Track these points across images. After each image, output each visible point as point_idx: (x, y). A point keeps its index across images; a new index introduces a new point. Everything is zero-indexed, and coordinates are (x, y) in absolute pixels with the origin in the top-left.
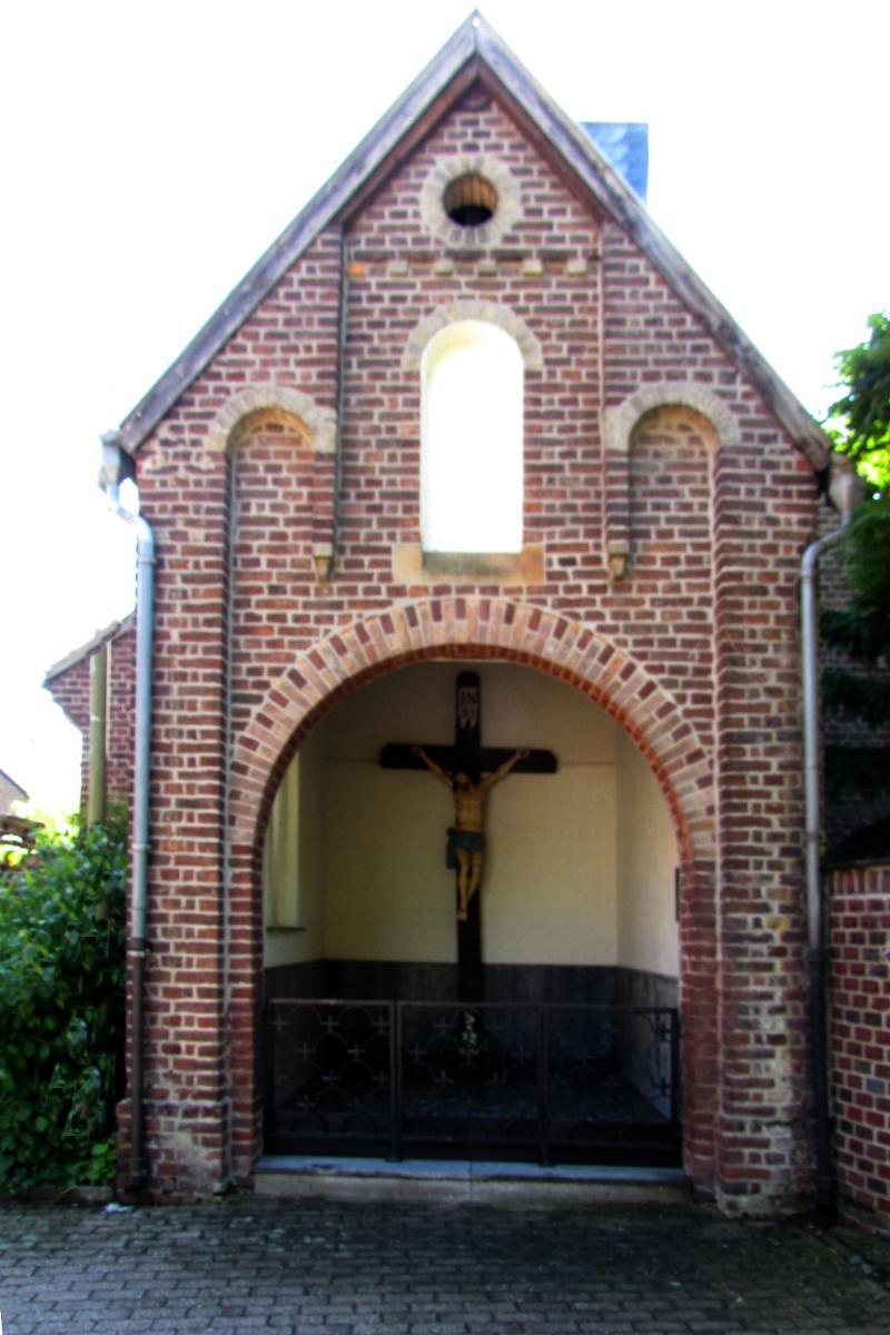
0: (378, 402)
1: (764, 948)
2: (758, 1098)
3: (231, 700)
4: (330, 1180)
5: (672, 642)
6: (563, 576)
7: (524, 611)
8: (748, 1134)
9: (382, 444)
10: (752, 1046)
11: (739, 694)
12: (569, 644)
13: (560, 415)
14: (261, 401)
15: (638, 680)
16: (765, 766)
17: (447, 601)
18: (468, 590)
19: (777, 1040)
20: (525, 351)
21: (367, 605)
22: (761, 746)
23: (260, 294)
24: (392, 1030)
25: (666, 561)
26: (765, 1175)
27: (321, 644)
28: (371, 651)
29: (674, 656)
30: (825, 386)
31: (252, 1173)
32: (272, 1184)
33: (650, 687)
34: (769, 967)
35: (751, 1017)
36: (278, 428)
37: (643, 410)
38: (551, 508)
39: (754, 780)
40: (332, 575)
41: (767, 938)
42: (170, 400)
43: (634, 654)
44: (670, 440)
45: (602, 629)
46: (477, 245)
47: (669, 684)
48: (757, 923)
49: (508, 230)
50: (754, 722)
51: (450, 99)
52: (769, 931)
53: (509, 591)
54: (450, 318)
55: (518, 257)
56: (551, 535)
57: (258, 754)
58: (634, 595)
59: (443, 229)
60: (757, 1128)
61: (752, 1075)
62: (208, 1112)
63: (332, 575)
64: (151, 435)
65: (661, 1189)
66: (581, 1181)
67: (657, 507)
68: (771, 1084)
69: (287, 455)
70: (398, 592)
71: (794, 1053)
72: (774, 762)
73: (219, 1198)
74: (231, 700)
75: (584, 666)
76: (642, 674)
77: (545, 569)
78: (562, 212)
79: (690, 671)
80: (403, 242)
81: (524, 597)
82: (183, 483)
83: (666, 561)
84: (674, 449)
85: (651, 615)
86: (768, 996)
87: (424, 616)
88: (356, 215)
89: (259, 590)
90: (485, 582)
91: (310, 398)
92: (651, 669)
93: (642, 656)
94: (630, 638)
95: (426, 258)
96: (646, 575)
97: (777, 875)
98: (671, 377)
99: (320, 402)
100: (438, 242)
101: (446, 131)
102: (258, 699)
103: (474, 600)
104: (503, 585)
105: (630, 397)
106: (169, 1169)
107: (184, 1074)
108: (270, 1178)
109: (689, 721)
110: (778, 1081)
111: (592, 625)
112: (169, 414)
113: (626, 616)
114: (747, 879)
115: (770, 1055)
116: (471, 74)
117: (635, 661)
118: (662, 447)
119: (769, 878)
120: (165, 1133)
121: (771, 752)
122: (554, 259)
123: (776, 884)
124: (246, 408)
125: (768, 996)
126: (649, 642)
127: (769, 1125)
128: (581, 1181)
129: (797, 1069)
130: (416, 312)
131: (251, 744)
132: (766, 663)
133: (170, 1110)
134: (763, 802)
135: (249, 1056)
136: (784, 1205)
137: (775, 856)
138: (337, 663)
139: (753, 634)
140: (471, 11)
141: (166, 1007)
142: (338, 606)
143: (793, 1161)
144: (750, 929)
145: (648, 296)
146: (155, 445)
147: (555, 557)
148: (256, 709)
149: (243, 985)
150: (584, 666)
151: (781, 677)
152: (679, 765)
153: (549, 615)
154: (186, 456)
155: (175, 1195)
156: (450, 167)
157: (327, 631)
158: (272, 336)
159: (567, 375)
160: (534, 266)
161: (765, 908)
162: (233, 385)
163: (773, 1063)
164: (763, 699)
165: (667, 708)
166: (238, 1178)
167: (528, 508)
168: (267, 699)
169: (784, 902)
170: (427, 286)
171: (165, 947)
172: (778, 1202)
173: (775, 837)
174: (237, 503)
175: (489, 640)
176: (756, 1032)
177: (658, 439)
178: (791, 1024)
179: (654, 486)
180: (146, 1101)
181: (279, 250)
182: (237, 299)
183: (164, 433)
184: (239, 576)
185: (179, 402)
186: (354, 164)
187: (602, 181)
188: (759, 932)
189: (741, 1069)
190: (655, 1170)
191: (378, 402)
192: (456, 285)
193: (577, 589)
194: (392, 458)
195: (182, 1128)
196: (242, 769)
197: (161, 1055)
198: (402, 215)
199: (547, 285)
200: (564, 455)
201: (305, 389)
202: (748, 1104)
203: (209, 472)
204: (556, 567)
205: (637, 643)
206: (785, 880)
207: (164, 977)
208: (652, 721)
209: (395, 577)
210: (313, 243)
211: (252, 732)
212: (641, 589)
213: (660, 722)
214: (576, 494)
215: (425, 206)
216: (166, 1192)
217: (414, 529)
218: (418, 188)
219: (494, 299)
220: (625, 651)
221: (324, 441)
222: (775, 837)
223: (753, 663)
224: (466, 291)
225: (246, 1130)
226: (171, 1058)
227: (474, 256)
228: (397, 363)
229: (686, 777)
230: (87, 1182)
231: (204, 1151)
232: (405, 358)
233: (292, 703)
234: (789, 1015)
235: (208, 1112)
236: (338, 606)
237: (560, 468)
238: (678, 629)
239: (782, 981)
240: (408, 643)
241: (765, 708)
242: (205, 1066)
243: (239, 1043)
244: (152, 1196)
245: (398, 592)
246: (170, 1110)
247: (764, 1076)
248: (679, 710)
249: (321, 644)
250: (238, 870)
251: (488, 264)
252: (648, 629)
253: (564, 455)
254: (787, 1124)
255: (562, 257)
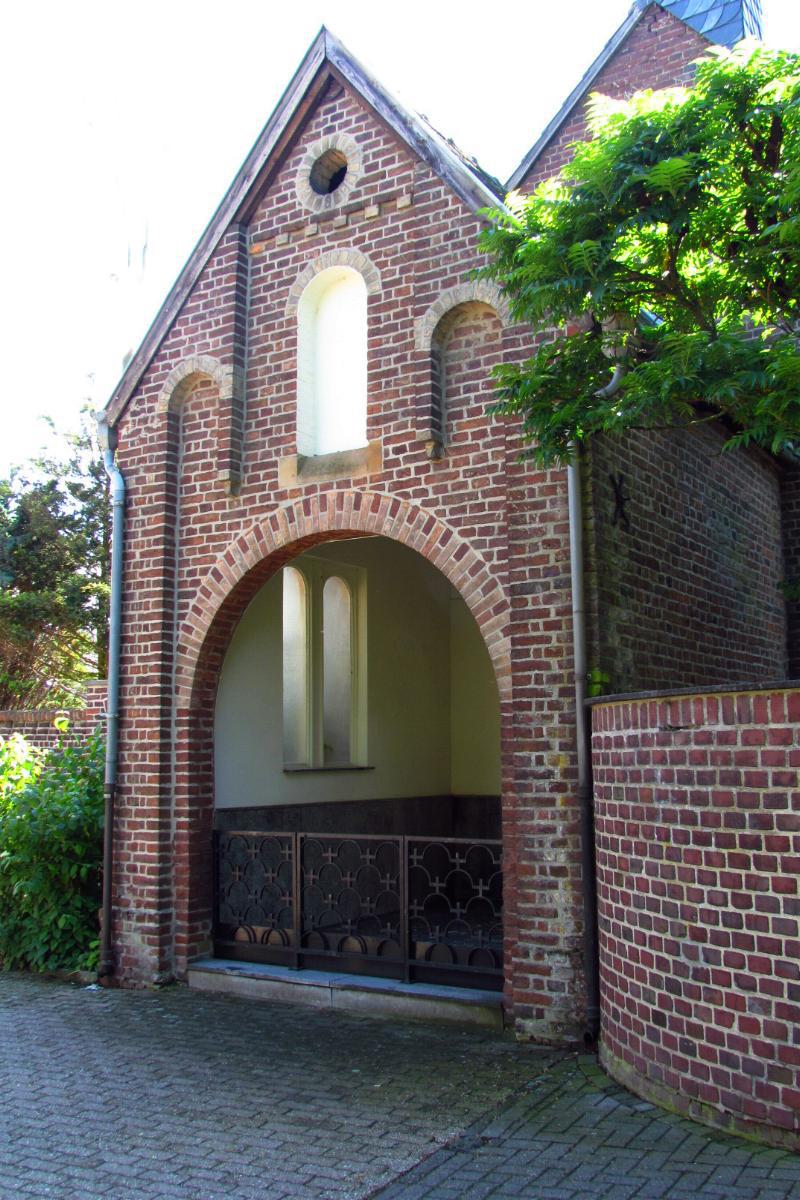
0: (269, 349)
1: (545, 783)
2: (542, 926)
3: (171, 594)
4: (236, 980)
5: (481, 507)
6: (396, 463)
7: (367, 499)
8: (531, 960)
9: (273, 380)
10: (537, 878)
11: (521, 549)
12: (401, 520)
13: (394, 328)
14: (189, 370)
15: (454, 545)
16: (545, 613)
17: (314, 497)
18: (328, 487)
19: (558, 871)
20: (368, 281)
21: (262, 510)
22: (540, 595)
23: (187, 291)
24: (294, 857)
25: (476, 436)
26: (547, 1001)
27: (232, 546)
28: (263, 546)
29: (482, 519)
30: (48, 419)
31: (187, 970)
32: (200, 980)
33: (464, 549)
34: (551, 802)
35: (536, 849)
36: (206, 383)
37: (443, 313)
38: (387, 407)
39: (536, 627)
40: (234, 492)
41: (549, 774)
42: (134, 384)
43: (450, 522)
44: (478, 329)
45: (426, 504)
46: (334, 207)
47: (478, 545)
48: (540, 761)
49: (354, 189)
50: (534, 573)
51: (310, 100)
52: (551, 767)
53: (357, 483)
54: (318, 269)
55: (361, 207)
56: (387, 430)
57: (193, 637)
58: (451, 470)
59: (309, 203)
60: (539, 956)
61: (537, 905)
62: (151, 918)
63: (234, 492)
64: (125, 409)
65: (477, 1009)
66: (411, 996)
67: (468, 390)
68: (555, 915)
69: (211, 403)
70: (282, 496)
71: (574, 884)
72: (552, 608)
73: (157, 987)
74: (171, 594)
75: (412, 538)
76: (457, 539)
77: (383, 459)
78: (391, 161)
79: (496, 531)
80: (284, 219)
81: (368, 485)
82: (143, 441)
83: (476, 436)
84: (481, 335)
85: (464, 485)
86: (551, 830)
87: (299, 514)
88: (253, 209)
89: (194, 510)
90: (340, 478)
91: (218, 359)
92: (463, 533)
93: (456, 523)
94: (447, 508)
95: (299, 227)
96: (458, 450)
97: (556, 714)
98: (465, 279)
99: (224, 362)
100: (307, 212)
101: (313, 123)
102: (193, 595)
103: (332, 494)
104: (352, 479)
105: (432, 304)
106: (127, 961)
107: (139, 888)
108: (197, 974)
109: (495, 576)
110: (560, 912)
111: (417, 502)
112: (136, 391)
113: (444, 489)
114: (530, 719)
115: (554, 886)
116: (325, 75)
117: (451, 528)
118: (472, 336)
119: (550, 718)
120: (126, 933)
121: (549, 600)
122: (385, 201)
123: (556, 723)
124: (180, 377)
125: (551, 830)
126: (463, 510)
127: (551, 953)
128: (411, 996)
129: (577, 900)
130: (294, 270)
131: (188, 629)
132: (544, 518)
133: (129, 915)
134: (543, 647)
135: (186, 876)
136: (566, 1032)
137: (555, 697)
138: (242, 559)
139: (532, 493)
140: (320, 28)
141: (129, 836)
142: (242, 514)
143: (572, 990)
144: (533, 767)
145: (447, 215)
146: (128, 417)
147: (390, 447)
148: (192, 602)
149: (183, 819)
150: (412, 538)
151: (557, 529)
152: (487, 617)
153: (386, 497)
154: (145, 421)
155: (132, 981)
156: (315, 151)
157: (236, 535)
158: (196, 319)
159: (399, 292)
160: (372, 211)
161: (547, 746)
162: (173, 361)
163: (556, 894)
164: (541, 552)
165: (480, 565)
166: (179, 974)
167: (370, 410)
168: (199, 594)
169: (563, 740)
170: (303, 247)
171: (129, 790)
172: (560, 1029)
173: (554, 679)
174: (183, 445)
175: (343, 527)
176: (541, 864)
177: (467, 330)
178: (571, 857)
179: (466, 371)
180: (114, 907)
181: (197, 252)
182: (172, 296)
183: (133, 407)
184: (184, 501)
185: (141, 381)
186: (243, 174)
187: (410, 131)
188: (541, 769)
189: (529, 899)
190: (481, 992)
191: (269, 349)
192: (321, 242)
193: (407, 472)
194: (279, 390)
195: (136, 929)
196: (182, 649)
197: (126, 873)
198: (284, 198)
199: (385, 222)
200: (398, 360)
201: (213, 354)
202: (534, 932)
203: (158, 429)
204: (392, 456)
205: (452, 512)
206: (563, 719)
207: (128, 813)
208: (465, 580)
209: (280, 485)
210: (220, 242)
211: (190, 619)
212: (456, 464)
213: (472, 579)
214: (406, 391)
215: (298, 186)
216: (126, 979)
217: (292, 444)
218: (294, 174)
219: (347, 244)
220: (443, 520)
221: (225, 393)
222: (554, 679)
223: (532, 519)
224: (329, 244)
225: (184, 935)
226: (131, 875)
227: (331, 216)
228: (282, 314)
229: (493, 627)
230: (86, 969)
231: (149, 949)
232: (286, 309)
233: (213, 594)
234: (570, 848)
235: (151, 918)
236: (242, 514)
237: (394, 372)
238: (485, 494)
239: (564, 815)
240: (288, 536)
241: (544, 559)
242: (150, 882)
243: (180, 865)
244: (118, 981)
245: (282, 496)
246: (129, 915)
247: (548, 906)
248: (487, 568)
249: (232, 546)
250: (181, 729)
251: (341, 219)
252: (461, 498)
253: (398, 360)
254: (567, 954)
255: (392, 198)
